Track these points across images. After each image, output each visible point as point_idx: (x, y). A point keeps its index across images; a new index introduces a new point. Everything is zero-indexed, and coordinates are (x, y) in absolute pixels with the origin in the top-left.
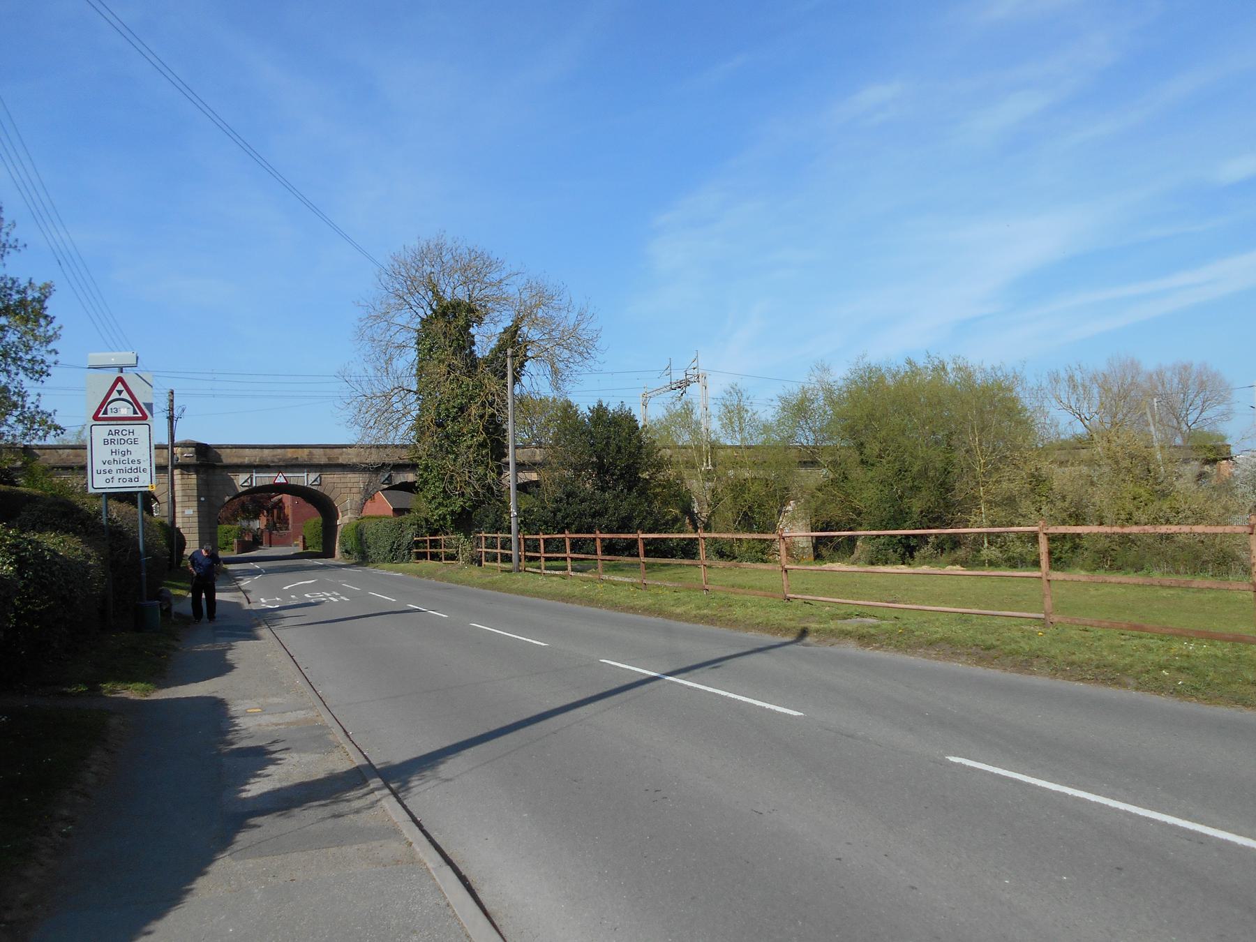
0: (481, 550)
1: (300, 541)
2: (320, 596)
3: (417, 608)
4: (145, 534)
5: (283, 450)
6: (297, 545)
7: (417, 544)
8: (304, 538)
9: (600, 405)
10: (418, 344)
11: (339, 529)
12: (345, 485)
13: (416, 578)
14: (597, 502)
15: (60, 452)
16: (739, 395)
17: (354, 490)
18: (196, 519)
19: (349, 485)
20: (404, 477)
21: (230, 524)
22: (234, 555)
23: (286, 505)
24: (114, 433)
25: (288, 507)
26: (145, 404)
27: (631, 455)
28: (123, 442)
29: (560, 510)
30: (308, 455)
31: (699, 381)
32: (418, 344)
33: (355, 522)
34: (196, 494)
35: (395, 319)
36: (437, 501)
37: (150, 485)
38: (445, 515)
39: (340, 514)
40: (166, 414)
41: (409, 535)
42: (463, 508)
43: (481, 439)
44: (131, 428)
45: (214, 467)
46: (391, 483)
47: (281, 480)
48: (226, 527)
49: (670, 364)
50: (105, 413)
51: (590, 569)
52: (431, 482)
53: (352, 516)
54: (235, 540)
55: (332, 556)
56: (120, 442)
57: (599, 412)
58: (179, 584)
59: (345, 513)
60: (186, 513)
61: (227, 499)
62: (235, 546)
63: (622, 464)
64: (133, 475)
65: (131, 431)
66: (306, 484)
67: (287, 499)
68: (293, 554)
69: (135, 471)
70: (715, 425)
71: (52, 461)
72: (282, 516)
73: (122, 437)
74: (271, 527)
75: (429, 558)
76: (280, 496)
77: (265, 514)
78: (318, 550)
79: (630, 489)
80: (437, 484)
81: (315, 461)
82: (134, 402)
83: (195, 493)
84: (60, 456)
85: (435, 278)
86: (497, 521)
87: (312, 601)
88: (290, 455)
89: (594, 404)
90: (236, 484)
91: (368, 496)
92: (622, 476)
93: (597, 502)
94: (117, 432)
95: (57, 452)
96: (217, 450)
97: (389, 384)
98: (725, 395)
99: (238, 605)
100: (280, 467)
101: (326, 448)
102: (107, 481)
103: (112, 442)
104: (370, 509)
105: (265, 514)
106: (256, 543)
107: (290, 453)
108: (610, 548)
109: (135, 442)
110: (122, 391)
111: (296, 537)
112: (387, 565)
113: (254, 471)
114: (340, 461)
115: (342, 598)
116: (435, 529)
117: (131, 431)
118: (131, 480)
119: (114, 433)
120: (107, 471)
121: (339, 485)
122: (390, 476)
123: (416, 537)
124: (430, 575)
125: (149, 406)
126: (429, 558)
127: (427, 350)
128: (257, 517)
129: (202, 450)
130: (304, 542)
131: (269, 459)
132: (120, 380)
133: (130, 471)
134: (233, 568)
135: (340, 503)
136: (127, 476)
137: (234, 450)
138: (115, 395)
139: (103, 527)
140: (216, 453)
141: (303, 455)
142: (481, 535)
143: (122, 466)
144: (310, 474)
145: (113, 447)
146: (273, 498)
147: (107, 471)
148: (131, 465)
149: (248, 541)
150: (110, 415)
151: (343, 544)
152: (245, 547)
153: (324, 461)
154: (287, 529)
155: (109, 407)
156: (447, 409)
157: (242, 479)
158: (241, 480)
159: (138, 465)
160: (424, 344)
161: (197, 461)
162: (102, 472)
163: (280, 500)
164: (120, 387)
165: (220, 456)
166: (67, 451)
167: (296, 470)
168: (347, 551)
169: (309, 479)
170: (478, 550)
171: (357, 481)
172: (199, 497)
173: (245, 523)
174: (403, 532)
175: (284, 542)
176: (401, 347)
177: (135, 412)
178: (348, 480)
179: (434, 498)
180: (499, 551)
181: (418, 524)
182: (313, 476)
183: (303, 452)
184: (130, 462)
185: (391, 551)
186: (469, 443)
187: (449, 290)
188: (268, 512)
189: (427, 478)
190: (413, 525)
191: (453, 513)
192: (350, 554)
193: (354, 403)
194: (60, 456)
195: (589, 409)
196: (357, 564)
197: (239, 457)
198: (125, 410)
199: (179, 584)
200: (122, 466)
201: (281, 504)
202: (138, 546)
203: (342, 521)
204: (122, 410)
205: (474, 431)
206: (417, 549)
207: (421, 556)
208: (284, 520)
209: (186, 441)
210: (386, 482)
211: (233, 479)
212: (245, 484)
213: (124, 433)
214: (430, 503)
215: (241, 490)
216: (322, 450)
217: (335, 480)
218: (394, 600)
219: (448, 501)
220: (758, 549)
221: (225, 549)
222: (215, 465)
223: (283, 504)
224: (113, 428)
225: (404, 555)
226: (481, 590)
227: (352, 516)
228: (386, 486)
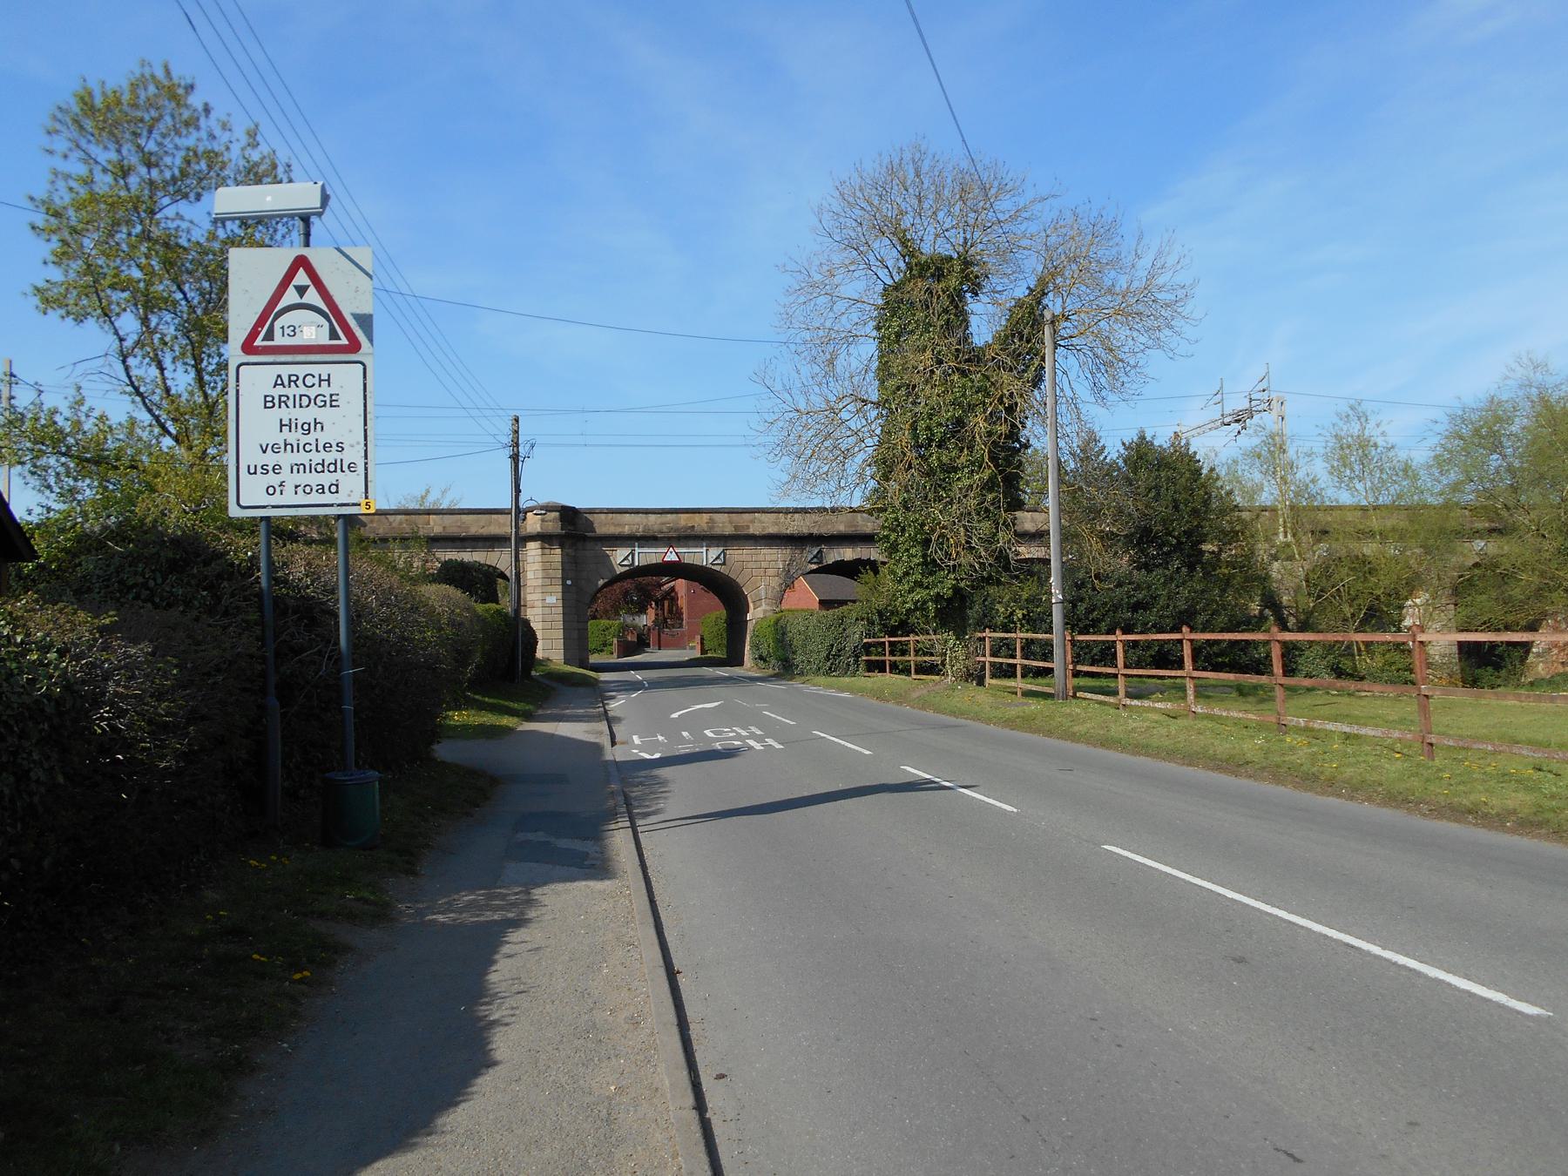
0: (983, 659)
1: (696, 643)
2: (731, 735)
3: (928, 777)
4: (353, 622)
5: (674, 515)
6: (693, 648)
7: (867, 648)
8: (702, 639)
9: (1142, 438)
10: (878, 328)
11: (750, 626)
12: (758, 565)
13: (874, 701)
14: (1138, 588)
15: (391, 518)
16: (1363, 420)
17: (771, 572)
18: (560, 610)
19: (764, 565)
20: (839, 553)
21: (609, 619)
22: (614, 659)
23: (679, 596)
24: (286, 383)
25: (682, 597)
26: (356, 317)
27: (1195, 512)
28: (305, 401)
29: (1082, 600)
30: (707, 523)
31: (1271, 410)
32: (878, 328)
33: (773, 617)
34: (560, 576)
35: (841, 288)
36: (912, 578)
37: (363, 502)
38: (925, 602)
39: (751, 605)
40: (509, 451)
41: (856, 634)
42: (956, 590)
43: (986, 475)
44: (324, 370)
45: (584, 539)
46: (821, 562)
47: (671, 557)
48: (604, 622)
49: (1222, 388)
50: (270, 336)
51: (1153, 693)
52: (902, 548)
53: (768, 608)
54: (615, 641)
55: (740, 663)
56: (298, 402)
57: (1141, 454)
58: (512, 705)
59: (758, 603)
60: (547, 601)
61: (601, 582)
62: (615, 647)
63: (1179, 528)
64: (326, 479)
65: (324, 377)
66: (705, 564)
67: (681, 585)
68: (687, 661)
69: (332, 468)
70: (1320, 468)
71: (381, 531)
72: (674, 609)
73: (303, 390)
74: (661, 623)
75: (888, 670)
76: (672, 584)
77: (653, 606)
78: (721, 654)
79: (1192, 568)
80: (913, 551)
81: (717, 531)
82: (332, 311)
83: (559, 574)
84: (391, 523)
85: (906, 222)
86: (985, 616)
87: (718, 746)
88: (683, 523)
89: (1131, 436)
90: (613, 562)
91: (788, 584)
92: (1179, 547)
93: (1138, 588)
94: (293, 380)
95: (387, 518)
96: (587, 515)
97: (837, 389)
98: (1336, 420)
99: (597, 748)
100: (669, 538)
101: (733, 513)
102: (270, 492)
103: (283, 401)
104: (792, 601)
105: (653, 606)
106: (641, 644)
107: (683, 520)
108: (1208, 658)
109: (332, 402)
110: (307, 287)
111: (692, 638)
112: (822, 679)
113: (636, 544)
114: (751, 531)
115: (770, 741)
116: (893, 626)
117: (324, 377)
118: (321, 489)
119: (286, 383)
120: (270, 468)
121: (750, 565)
122: (820, 552)
123: (866, 637)
124: (900, 698)
125: (366, 321)
126: (888, 670)
127: (892, 335)
128: (642, 610)
129: (569, 515)
130: (702, 644)
131: (656, 528)
132: (301, 262)
133: (319, 468)
134: (606, 679)
135: (751, 590)
136: (314, 479)
137: (611, 515)
138: (290, 297)
139: (260, 595)
140: (587, 519)
141: (700, 522)
142: (984, 634)
143: (302, 458)
144: (711, 550)
145: (285, 413)
146: (663, 585)
147: (270, 468)
148: (323, 455)
149: (631, 641)
150: (279, 340)
151: (755, 646)
152: (628, 649)
153: (729, 530)
154: (681, 626)
155: (278, 324)
156: (928, 428)
157: (621, 556)
158: (620, 557)
159: (339, 456)
160: (889, 327)
161: (562, 529)
162: (259, 470)
163: (673, 589)
164: (301, 278)
165: (592, 523)
166: (399, 517)
167: (690, 543)
168: (761, 658)
169: (709, 556)
170: (978, 659)
171: (775, 558)
172: (564, 579)
173: (629, 619)
174: (844, 630)
175: (678, 644)
176: (851, 338)
177: (333, 335)
178: (761, 557)
179: (906, 574)
180: (1018, 661)
181: (868, 619)
182: (714, 552)
183: (702, 518)
184: (320, 448)
185: (828, 658)
186: (967, 482)
187: (929, 238)
188: (657, 604)
189: (896, 541)
190: (862, 620)
191: (938, 598)
192: (765, 661)
193: (781, 424)
194: (391, 523)
195: (1124, 444)
196: (777, 676)
197: (619, 525)
198: (313, 330)
199: (512, 705)
200: (302, 458)
201: (673, 594)
202: (337, 643)
203: (754, 615)
204: (305, 329)
205: (973, 463)
206: (867, 656)
207: (880, 667)
208: (678, 615)
209: (549, 503)
210: (815, 560)
211: (608, 556)
212: (625, 563)
213: (309, 381)
214: (900, 582)
215: (619, 570)
216: (726, 515)
217: (744, 558)
218: (868, 752)
219: (931, 579)
220: (1400, 666)
221: (602, 651)
222: (586, 536)
223: (676, 594)
224: (285, 371)
225: (848, 665)
226: (1007, 731)
227: (768, 608)
228: (814, 567)
